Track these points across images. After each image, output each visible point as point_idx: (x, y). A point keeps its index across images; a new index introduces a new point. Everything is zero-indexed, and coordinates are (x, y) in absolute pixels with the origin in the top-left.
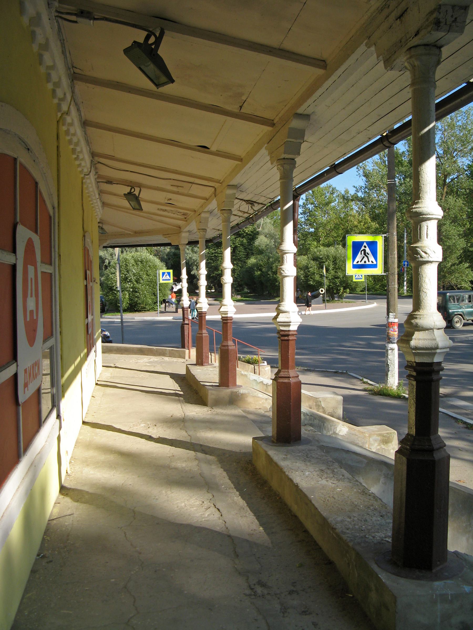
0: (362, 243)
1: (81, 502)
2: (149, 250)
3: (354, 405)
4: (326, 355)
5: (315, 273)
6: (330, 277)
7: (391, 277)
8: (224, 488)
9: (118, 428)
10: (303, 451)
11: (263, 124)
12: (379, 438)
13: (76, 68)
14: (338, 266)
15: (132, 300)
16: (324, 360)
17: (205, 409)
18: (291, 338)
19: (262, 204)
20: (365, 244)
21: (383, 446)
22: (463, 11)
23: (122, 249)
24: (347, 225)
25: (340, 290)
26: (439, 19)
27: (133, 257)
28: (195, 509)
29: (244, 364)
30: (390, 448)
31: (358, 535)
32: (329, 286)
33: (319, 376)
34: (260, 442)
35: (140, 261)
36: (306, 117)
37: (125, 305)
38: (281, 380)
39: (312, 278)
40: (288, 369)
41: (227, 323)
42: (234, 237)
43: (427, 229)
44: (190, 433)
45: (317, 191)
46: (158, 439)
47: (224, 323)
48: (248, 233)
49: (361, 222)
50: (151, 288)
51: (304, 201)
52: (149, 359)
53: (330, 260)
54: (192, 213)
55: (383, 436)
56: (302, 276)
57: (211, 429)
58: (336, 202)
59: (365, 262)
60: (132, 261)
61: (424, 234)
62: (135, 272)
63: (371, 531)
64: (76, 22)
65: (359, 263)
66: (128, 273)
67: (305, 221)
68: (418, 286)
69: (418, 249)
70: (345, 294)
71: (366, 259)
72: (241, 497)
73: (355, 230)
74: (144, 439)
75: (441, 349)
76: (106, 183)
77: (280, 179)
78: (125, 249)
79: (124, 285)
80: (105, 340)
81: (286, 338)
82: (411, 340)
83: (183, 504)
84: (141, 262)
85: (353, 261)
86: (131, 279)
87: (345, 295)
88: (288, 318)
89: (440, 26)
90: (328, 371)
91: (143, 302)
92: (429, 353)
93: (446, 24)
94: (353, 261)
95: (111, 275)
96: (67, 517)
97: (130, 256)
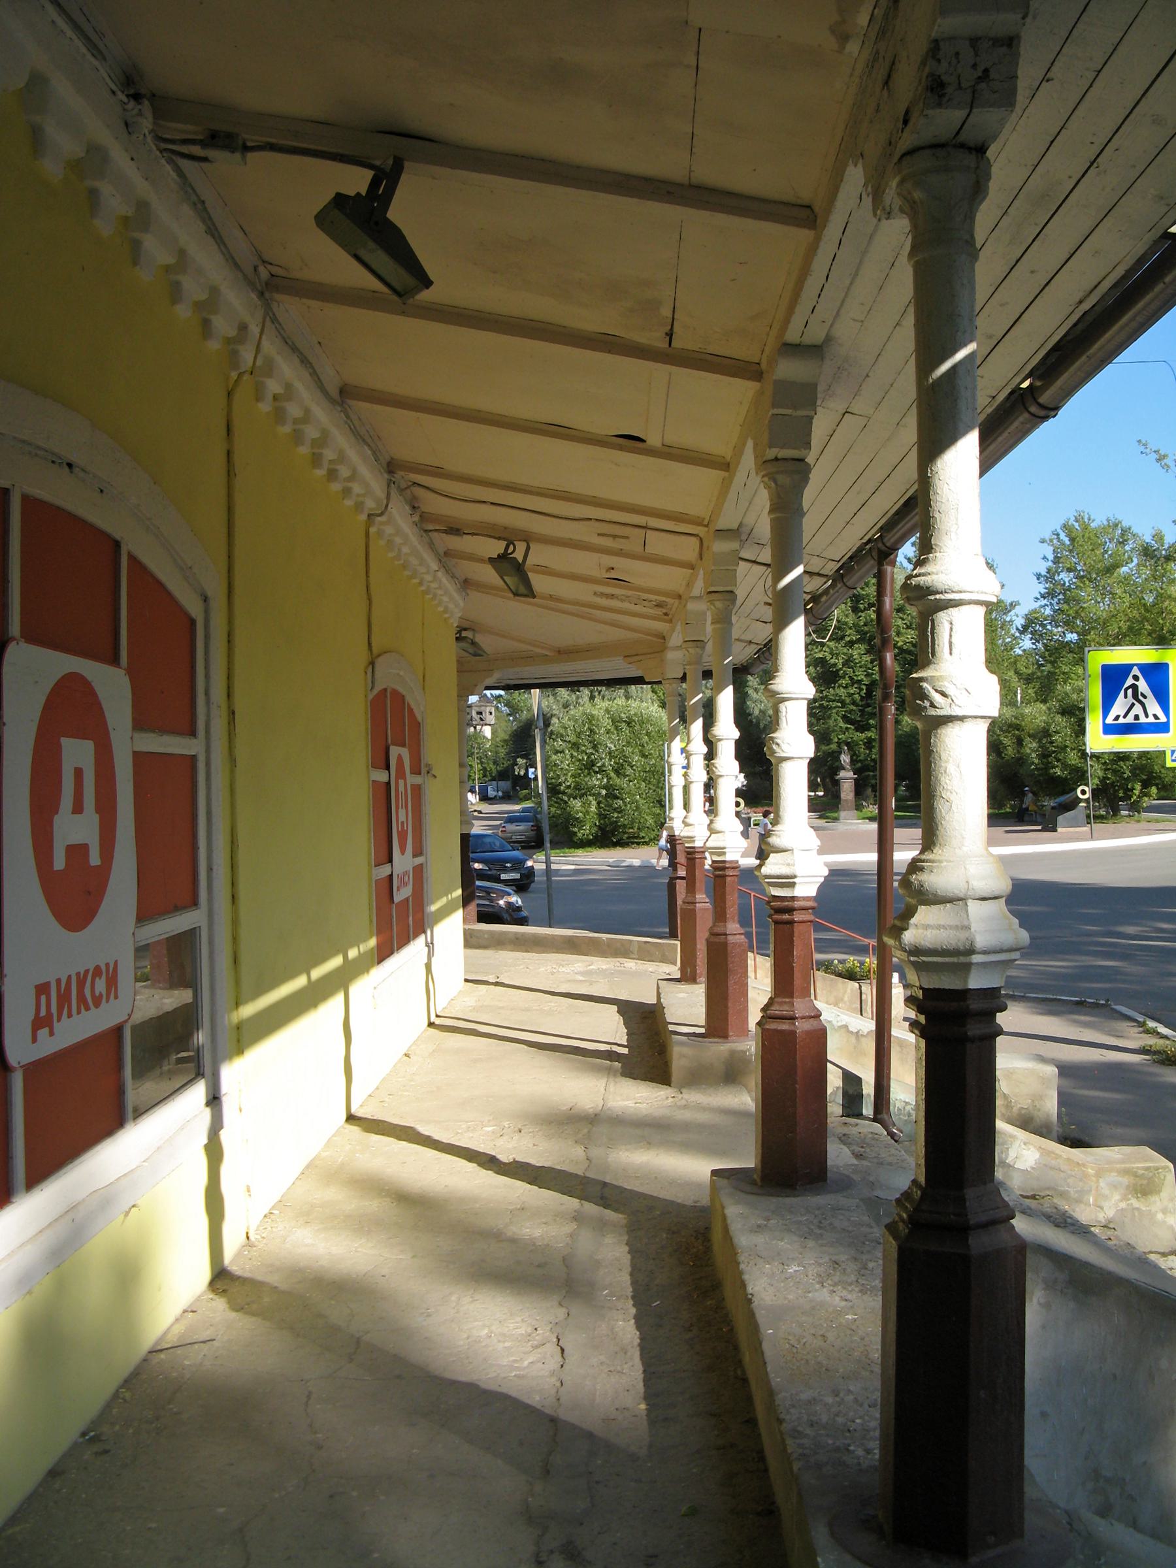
1: (247, 1313)
2: (661, 694)
3: (1101, 1089)
4: (1067, 957)
5: (1067, 747)
8: (606, 1295)
9: (426, 1133)
10: (819, 1209)
11: (734, 375)
12: (1125, 1180)
13: (271, 264)
15: (605, 817)
16: (1058, 970)
17: (662, 1093)
18: (797, 917)
19: (819, 575)
21: (1135, 1203)
22: (1004, 49)
23: (591, 692)
24: (1161, 621)
25: (1133, 789)
26: (939, 76)
27: (607, 711)
28: (507, 1344)
29: (832, 980)
30: (1153, 1209)
31: (830, 1442)
32: (1103, 780)
33: (1033, 1013)
34: (723, 1182)
35: (625, 721)
36: (815, 351)
37: (586, 831)
38: (773, 1026)
39: (1058, 760)
40: (791, 996)
41: (725, 876)
42: (869, 659)
43: (951, 629)
44: (596, 1152)
45: (1083, 536)
46: (510, 1163)
47: (716, 876)
48: (905, 647)
50: (651, 787)
51: (1050, 564)
52: (588, 963)
54: (677, 602)
55: (1136, 1175)
56: (1034, 755)
57: (649, 1144)
58: (1133, 564)
59: (1137, 717)
60: (606, 722)
61: (941, 645)
62: (613, 748)
63: (872, 1433)
64: (205, 159)
65: (1121, 721)
66: (597, 751)
67: (1052, 616)
68: (930, 785)
69: (925, 685)
70: (1146, 799)
71: (1138, 710)
72: (636, 1323)
74: (475, 1165)
75: (985, 953)
76: (445, 532)
77: (771, 511)
78: (599, 693)
79: (586, 779)
80: (511, 915)
81: (786, 917)
82: (906, 929)
83: (486, 1331)
84: (629, 723)
85: (1105, 716)
86: (603, 765)
87: (1146, 802)
88: (788, 865)
89: (943, 95)
90: (1060, 1000)
91: (633, 822)
92: (953, 963)
93: (960, 88)
94: (1105, 715)
95: (554, 757)
96: (196, 1346)
97: (601, 709)
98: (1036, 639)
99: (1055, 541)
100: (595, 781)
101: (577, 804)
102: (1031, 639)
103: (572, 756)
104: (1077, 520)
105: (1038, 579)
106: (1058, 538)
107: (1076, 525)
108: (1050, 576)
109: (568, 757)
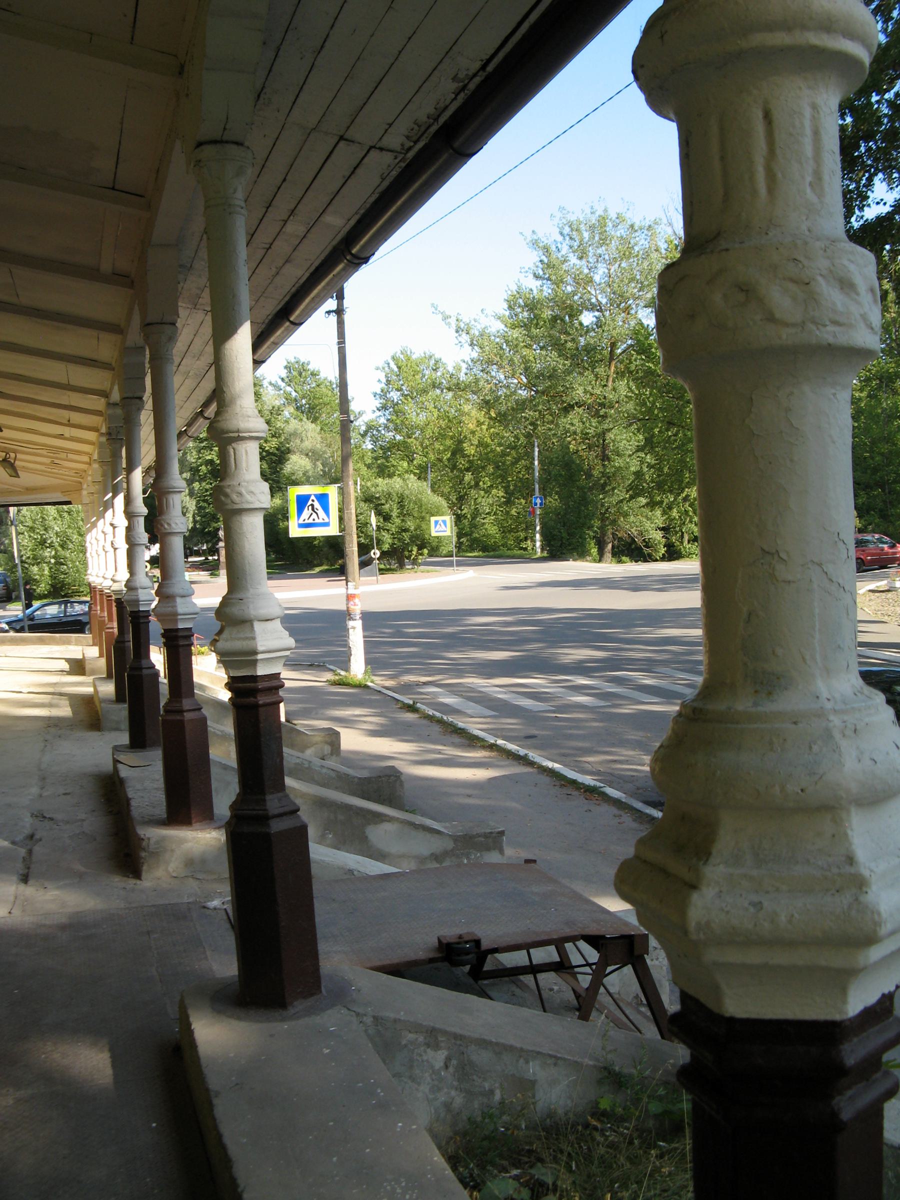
0: (309, 496)
6: (393, 530)
7: (347, 538)
14: (407, 511)
15: (55, 578)
20: (313, 497)
24: (459, 429)
35: (67, 511)
37: (42, 588)
45: (407, 365)
49: (483, 424)
53: (392, 501)
59: (314, 520)
65: (307, 521)
73: (470, 440)
86: (52, 542)
87: (420, 559)
98: (373, 441)
99: (387, 369)
100: (48, 553)
101: (35, 569)
102: (370, 441)
103: (30, 537)
104: (402, 353)
105: (375, 396)
106: (389, 366)
107: (402, 356)
108: (384, 394)
109: (27, 537)
